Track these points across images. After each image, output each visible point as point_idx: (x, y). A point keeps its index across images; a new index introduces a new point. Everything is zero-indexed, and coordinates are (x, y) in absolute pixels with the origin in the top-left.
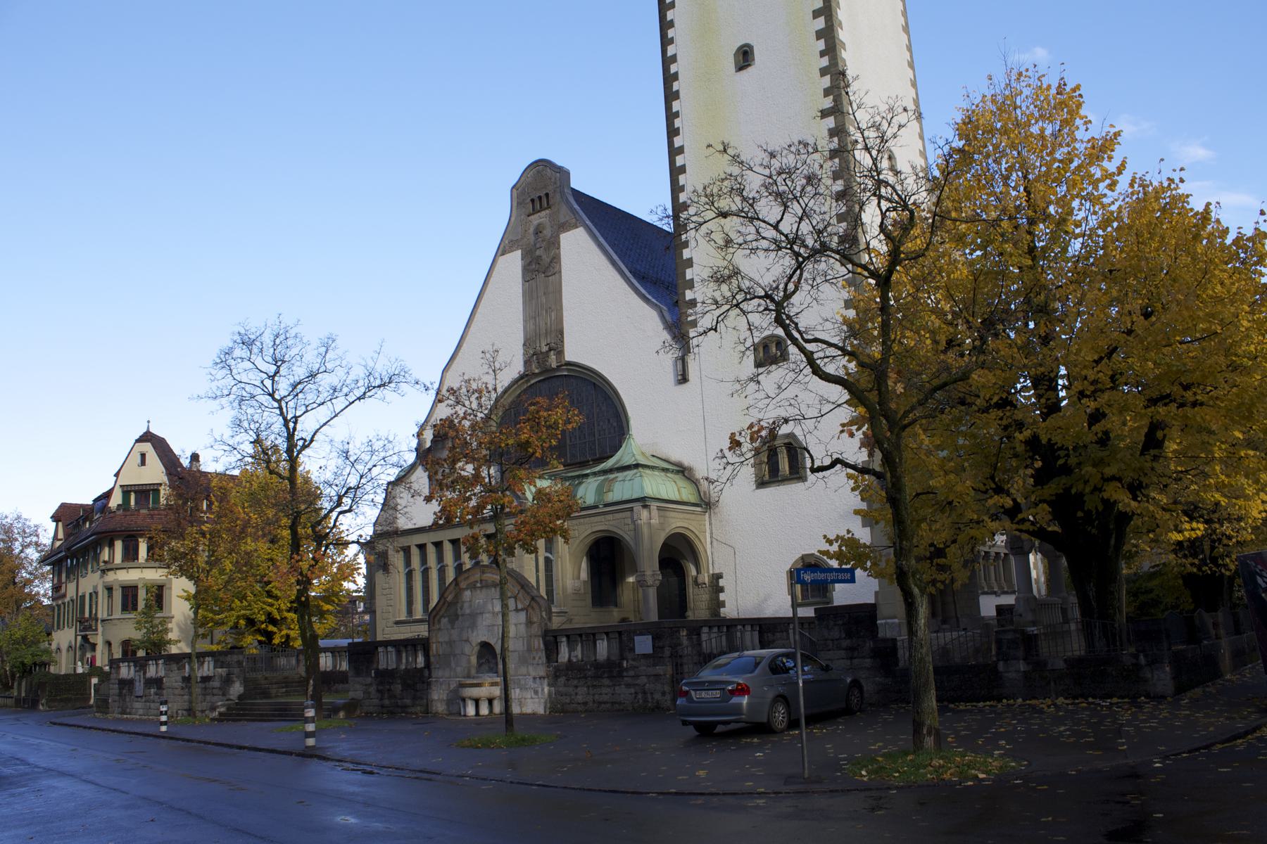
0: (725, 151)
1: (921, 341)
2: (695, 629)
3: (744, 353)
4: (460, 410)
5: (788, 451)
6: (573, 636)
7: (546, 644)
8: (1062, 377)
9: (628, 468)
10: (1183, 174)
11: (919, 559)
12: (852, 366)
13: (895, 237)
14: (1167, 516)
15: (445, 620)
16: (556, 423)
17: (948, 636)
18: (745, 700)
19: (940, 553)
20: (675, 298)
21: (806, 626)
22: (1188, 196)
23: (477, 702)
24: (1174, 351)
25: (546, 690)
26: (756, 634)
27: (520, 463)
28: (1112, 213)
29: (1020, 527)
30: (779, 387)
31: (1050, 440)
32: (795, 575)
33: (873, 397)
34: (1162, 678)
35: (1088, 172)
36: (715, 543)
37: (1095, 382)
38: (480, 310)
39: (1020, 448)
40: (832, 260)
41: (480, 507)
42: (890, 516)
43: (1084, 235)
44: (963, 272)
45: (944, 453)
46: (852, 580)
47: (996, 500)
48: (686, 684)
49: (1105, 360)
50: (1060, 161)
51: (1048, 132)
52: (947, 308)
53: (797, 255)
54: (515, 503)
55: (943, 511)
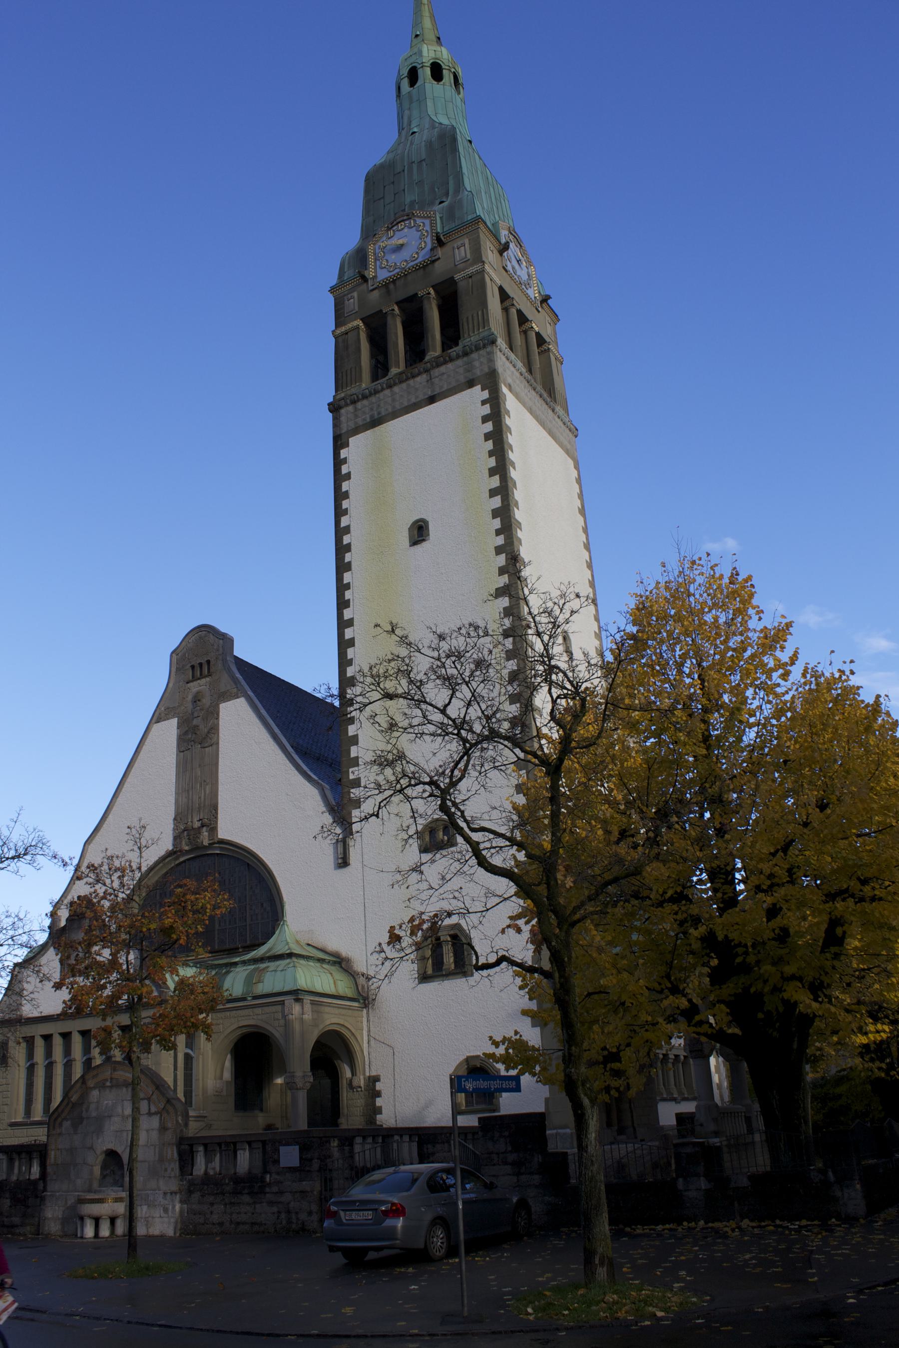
0: (393, 631)
1: (592, 830)
2: (347, 1140)
3: (406, 841)
4: (100, 889)
5: (453, 945)
6: (211, 1145)
7: (180, 1154)
8: (739, 870)
9: (281, 957)
10: (853, 666)
11: (591, 1064)
12: (521, 856)
13: (567, 721)
14: (849, 1018)
15: (66, 1124)
16: (204, 908)
17: (624, 1149)
18: (400, 1223)
19: (615, 1057)
20: (339, 776)
21: (470, 1136)
22: (858, 688)
23: (97, 1221)
24: (850, 844)
25: (178, 1207)
26: (415, 1146)
27: (162, 949)
28: (785, 703)
29: (699, 1030)
30: (443, 878)
31: (726, 936)
32: (456, 1084)
33: (542, 890)
34: (853, 1197)
35: (761, 661)
36: (372, 1042)
37: (771, 876)
38: (120, 800)
39: (696, 946)
40: (501, 747)
41: (115, 997)
42: (559, 1017)
43: (758, 724)
44: (636, 761)
45: (617, 950)
46: (518, 1089)
47: (670, 1001)
48: (335, 1204)
49: (780, 854)
50: (734, 650)
51: (722, 620)
52: (620, 797)
53: (465, 741)
54: (155, 994)
55: (616, 1012)
